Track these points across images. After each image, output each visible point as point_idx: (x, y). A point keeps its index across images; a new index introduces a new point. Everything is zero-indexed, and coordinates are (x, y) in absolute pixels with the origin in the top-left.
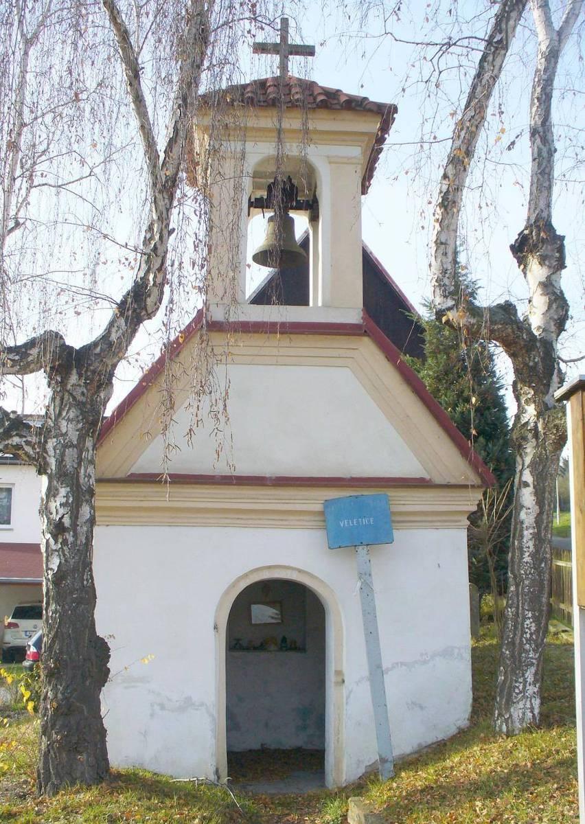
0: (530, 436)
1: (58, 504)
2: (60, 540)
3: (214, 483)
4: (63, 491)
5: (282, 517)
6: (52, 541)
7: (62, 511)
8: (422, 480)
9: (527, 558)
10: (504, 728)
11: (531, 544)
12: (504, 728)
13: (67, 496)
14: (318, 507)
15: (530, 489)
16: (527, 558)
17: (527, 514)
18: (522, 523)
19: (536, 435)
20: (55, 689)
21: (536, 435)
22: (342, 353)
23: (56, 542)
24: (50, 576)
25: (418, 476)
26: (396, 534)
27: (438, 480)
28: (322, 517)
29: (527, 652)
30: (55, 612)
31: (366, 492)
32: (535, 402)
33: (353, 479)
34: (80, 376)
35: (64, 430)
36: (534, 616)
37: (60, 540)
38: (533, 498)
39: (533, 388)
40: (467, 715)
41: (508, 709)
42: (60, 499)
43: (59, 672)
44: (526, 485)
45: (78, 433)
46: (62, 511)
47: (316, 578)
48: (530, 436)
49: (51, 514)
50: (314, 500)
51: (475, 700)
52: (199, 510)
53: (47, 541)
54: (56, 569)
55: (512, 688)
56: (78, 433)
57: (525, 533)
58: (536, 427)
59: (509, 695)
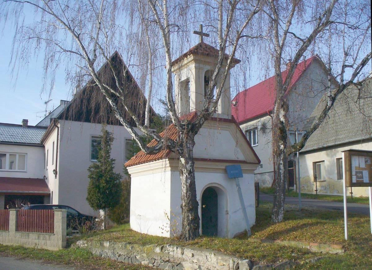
0: (282, 152)
1: (189, 166)
2: (190, 175)
3: (199, 160)
4: (190, 162)
5: (215, 170)
6: (188, 175)
7: (190, 168)
8: (244, 161)
9: (282, 181)
10: (277, 221)
11: (283, 178)
12: (277, 221)
13: (191, 164)
14: (224, 168)
15: (282, 165)
16: (282, 181)
17: (282, 171)
18: (281, 173)
19: (284, 153)
20: (191, 214)
21: (284, 153)
22: (227, 127)
23: (189, 175)
24: (188, 185)
25: (244, 160)
26: (244, 175)
27: (248, 162)
28: (226, 171)
29: (282, 203)
30: (190, 194)
31: (236, 164)
32: (283, 144)
33: (230, 160)
34: (192, 133)
35: (189, 146)
36: (283, 195)
37: (190, 175)
38: (283, 167)
39: (283, 141)
40: (255, 221)
41: (278, 217)
42: (189, 165)
43: (192, 209)
44: (281, 164)
45: (132, 139)
46: (190, 168)
47: (222, 186)
48: (282, 152)
49: (187, 168)
50: (223, 166)
51: (257, 218)
52: (208, 168)
53: (186, 175)
54: (189, 183)
55: (279, 212)
56: (132, 139)
57: (281, 175)
58: (284, 150)
59: (278, 213)
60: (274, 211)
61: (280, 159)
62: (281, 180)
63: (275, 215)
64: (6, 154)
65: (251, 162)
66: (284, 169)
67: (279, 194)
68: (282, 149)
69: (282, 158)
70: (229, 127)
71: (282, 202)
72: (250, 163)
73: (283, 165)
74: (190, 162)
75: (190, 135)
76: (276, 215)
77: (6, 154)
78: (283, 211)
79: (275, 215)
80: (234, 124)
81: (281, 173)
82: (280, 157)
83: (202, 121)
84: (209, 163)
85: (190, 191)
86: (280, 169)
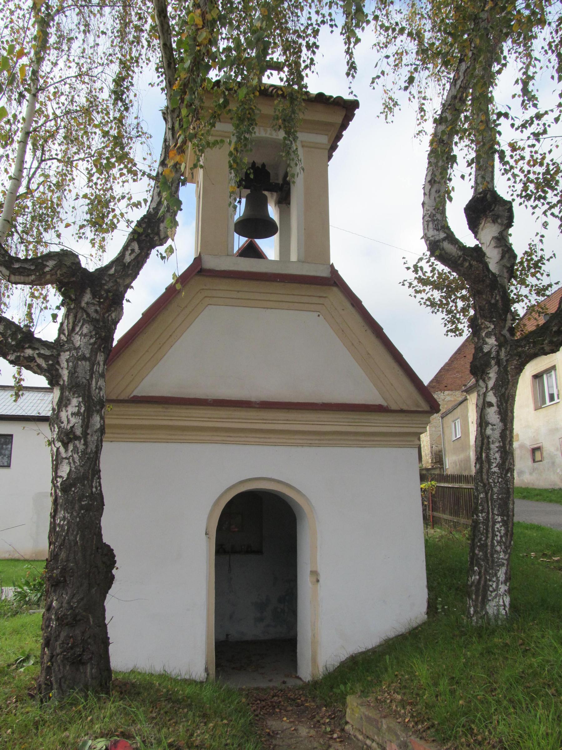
0: (493, 362)
4: (75, 401)
11: (497, 455)
17: (493, 430)
18: (488, 437)
19: (498, 363)
24: (59, 484)
36: (503, 521)
44: (490, 405)
53: (58, 449)
55: (486, 587)
57: (492, 446)
60: (473, 583)
61: (487, 387)
62: (490, 463)
63: (474, 597)
64: (11, 436)
65: (405, 408)
66: (501, 424)
67: (487, 519)
68: (489, 352)
69: (491, 384)
70: (321, 301)
71: (498, 548)
72: (402, 411)
73: (498, 407)
74: (75, 401)
75: (83, 304)
76: (477, 596)
77: (11, 436)
78: (505, 583)
79: (474, 597)
80: (335, 289)
81: (488, 437)
82: (484, 381)
83: (130, 254)
84: (252, 414)
85: (69, 505)
86: (487, 424)
